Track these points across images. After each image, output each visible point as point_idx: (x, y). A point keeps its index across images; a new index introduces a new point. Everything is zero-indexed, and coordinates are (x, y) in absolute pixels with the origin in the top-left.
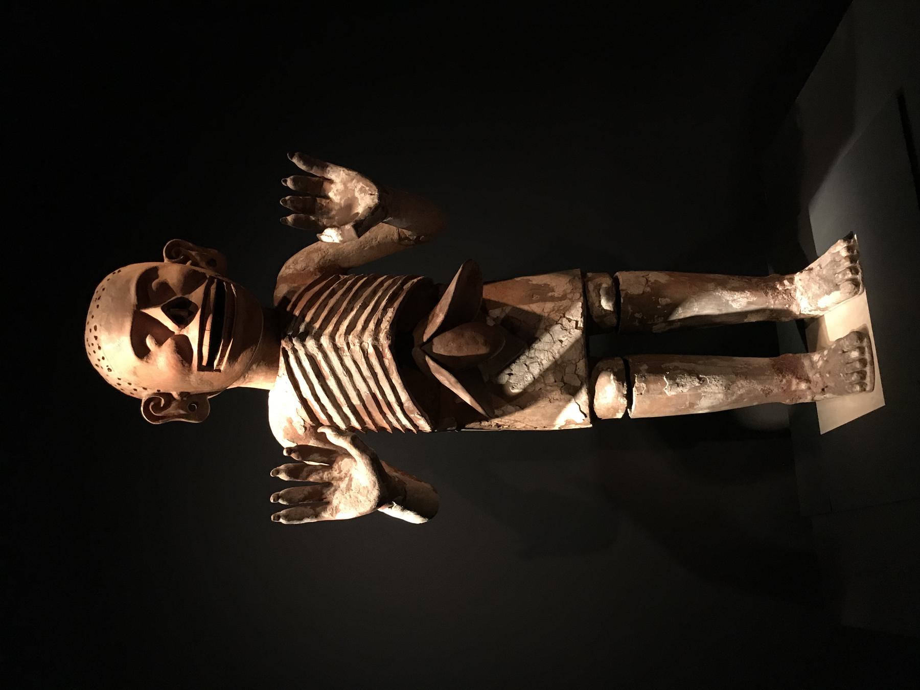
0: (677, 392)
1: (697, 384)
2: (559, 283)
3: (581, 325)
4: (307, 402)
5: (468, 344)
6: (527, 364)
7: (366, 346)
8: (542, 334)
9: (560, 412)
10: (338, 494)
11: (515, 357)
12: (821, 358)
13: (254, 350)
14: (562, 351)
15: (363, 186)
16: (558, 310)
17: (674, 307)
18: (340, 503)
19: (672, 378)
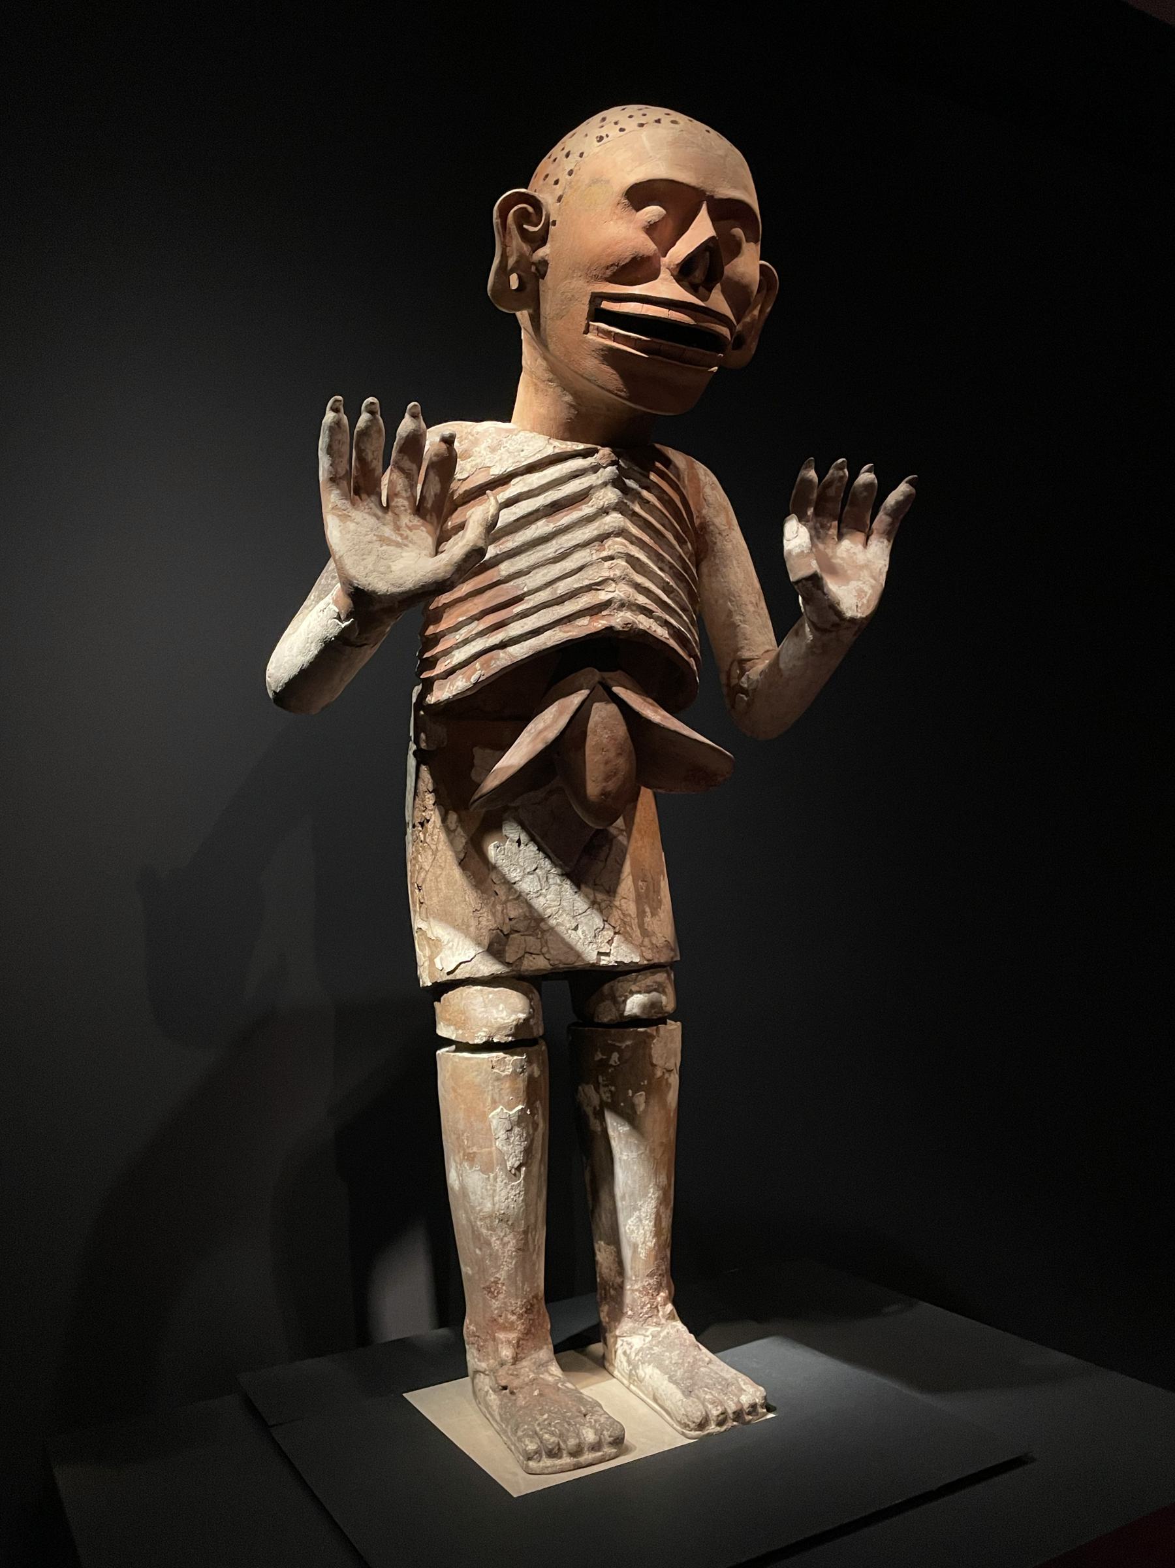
0: (496, 1129)
1: (509, 1164)
2: (662, 925)
3: (604, 961)
4: (503, 485)
5: (606, 763)
6: (537, 871)
7: (610, 589)
8: (587, 896)
9: (457, 928)
10: (372, 521)
11: (549, 851)
12: (557, 1378)
13: (619, 393)
14: (561, 929)
15: (868, 595)
16: (625, 923)
17: (630, 1117)
18: (357, 523)
19: (521, 1119)
